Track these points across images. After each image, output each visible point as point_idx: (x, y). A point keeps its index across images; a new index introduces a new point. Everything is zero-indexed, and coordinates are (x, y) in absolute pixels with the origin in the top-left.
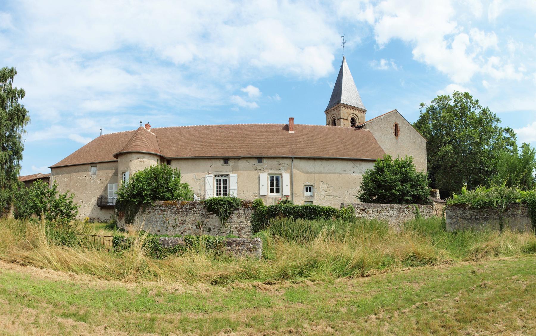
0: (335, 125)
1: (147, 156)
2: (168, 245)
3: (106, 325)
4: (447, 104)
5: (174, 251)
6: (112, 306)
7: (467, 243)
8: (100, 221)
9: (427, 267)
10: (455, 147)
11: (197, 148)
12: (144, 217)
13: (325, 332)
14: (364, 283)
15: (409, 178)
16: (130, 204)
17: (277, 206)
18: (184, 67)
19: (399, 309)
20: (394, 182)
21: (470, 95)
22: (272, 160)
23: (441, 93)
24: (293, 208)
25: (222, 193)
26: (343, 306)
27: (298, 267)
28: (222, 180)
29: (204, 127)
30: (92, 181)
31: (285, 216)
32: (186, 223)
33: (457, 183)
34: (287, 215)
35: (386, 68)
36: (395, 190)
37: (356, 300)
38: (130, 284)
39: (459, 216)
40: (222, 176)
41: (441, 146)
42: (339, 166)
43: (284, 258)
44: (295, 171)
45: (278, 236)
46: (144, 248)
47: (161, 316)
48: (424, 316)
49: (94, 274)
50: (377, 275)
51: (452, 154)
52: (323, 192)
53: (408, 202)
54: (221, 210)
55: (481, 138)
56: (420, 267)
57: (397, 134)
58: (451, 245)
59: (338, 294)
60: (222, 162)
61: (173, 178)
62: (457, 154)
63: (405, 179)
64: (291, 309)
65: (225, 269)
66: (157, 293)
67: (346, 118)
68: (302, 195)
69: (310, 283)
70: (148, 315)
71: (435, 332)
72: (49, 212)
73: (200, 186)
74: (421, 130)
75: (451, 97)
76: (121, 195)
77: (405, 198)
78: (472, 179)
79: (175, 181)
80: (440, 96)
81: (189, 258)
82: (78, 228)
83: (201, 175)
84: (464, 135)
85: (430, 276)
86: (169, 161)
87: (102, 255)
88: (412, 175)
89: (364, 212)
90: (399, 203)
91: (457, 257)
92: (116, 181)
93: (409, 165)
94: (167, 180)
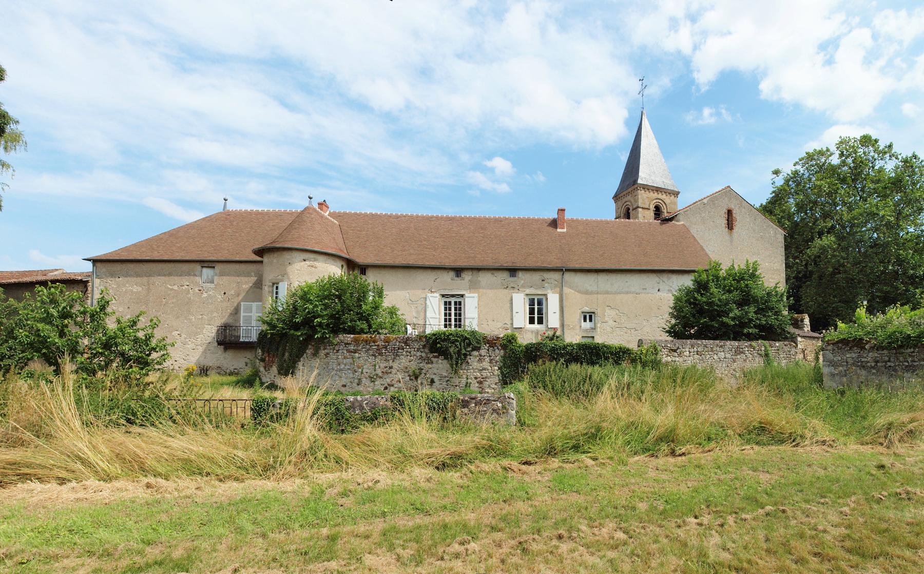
0: (629, 218)
1: (321, 258)
2: (362, 408)
3: (237, 565)
4: (824, 164)
5: (372, 418)
6: (249, 527)
7: (867, 412)
8: (220, 371)
9: (786, 448)
10: (840, 238)
11: (412, 251)
12: (317, 362)
13: (613, 538)
14: (676, 466)
15: (753, 297)
16: (292, 338)
17: (539, 344)
18: (388, 117)
19: (736, 513)
20: (727, 304)
21: (874, 138)
22: (531, 273)
23: (813, 146)
24: (565, 347)
25: (453, 322)
26: (641, 499)
27: (571, 438)
28: (453, 304)
29: (423, 217)
30: (205, 295)
31: (552, 359)
32: (394, 371)
33: (845, 302)
34: (554, 358)
35: (712, 120)
36: (728, 317)
37: (662, 491)
38: (288, 483)
39: (850, 361)
40: (453, 296)
41: (812, 240)
42: (635, 282)
43: (550, 423)
44: (566, 290)
45: (541, 390)
46: (316, 416)
47: (349, 528)
48: (780, 532)
49: (208, 474)
50: (697, 455)
51: (834, 250)
52: (611, 323)
53: (750, 337)
54: (451, 350)
55: (900, 213)
56: (773, 447)
57: (730, 225)
58: (834, 412)
59: (633, 481)
60: (452, 274)
61: (371, 298)
62: (845, 249)
63: (746, 299)
64: (561, 502)
65: (459, 443)
66: (341, 490)
67: (647, 206)
68: (578, 327)
69: (590, 462)
70: (325, 531)
71: (800, 561)
72: (86, 356)
73: (418, 312)
74: (775, 215)
75: (833, 149)
76: (269, 324)
77: (745, 331)
78: (879, 294)
79: (374, 302)
80: (811, 151)
81: (398, 427)
82: (168, 388)
83: (420, 293)
84: (861, 215)
85: (791, 464)
86: (363, 269)
87: (228, 435)
88: (758, 293)
89: (676, 354)
90: (735, 339)
91: (845, 435)
92: (260, 299)
93: (753, 276)
94: (359, 300)
